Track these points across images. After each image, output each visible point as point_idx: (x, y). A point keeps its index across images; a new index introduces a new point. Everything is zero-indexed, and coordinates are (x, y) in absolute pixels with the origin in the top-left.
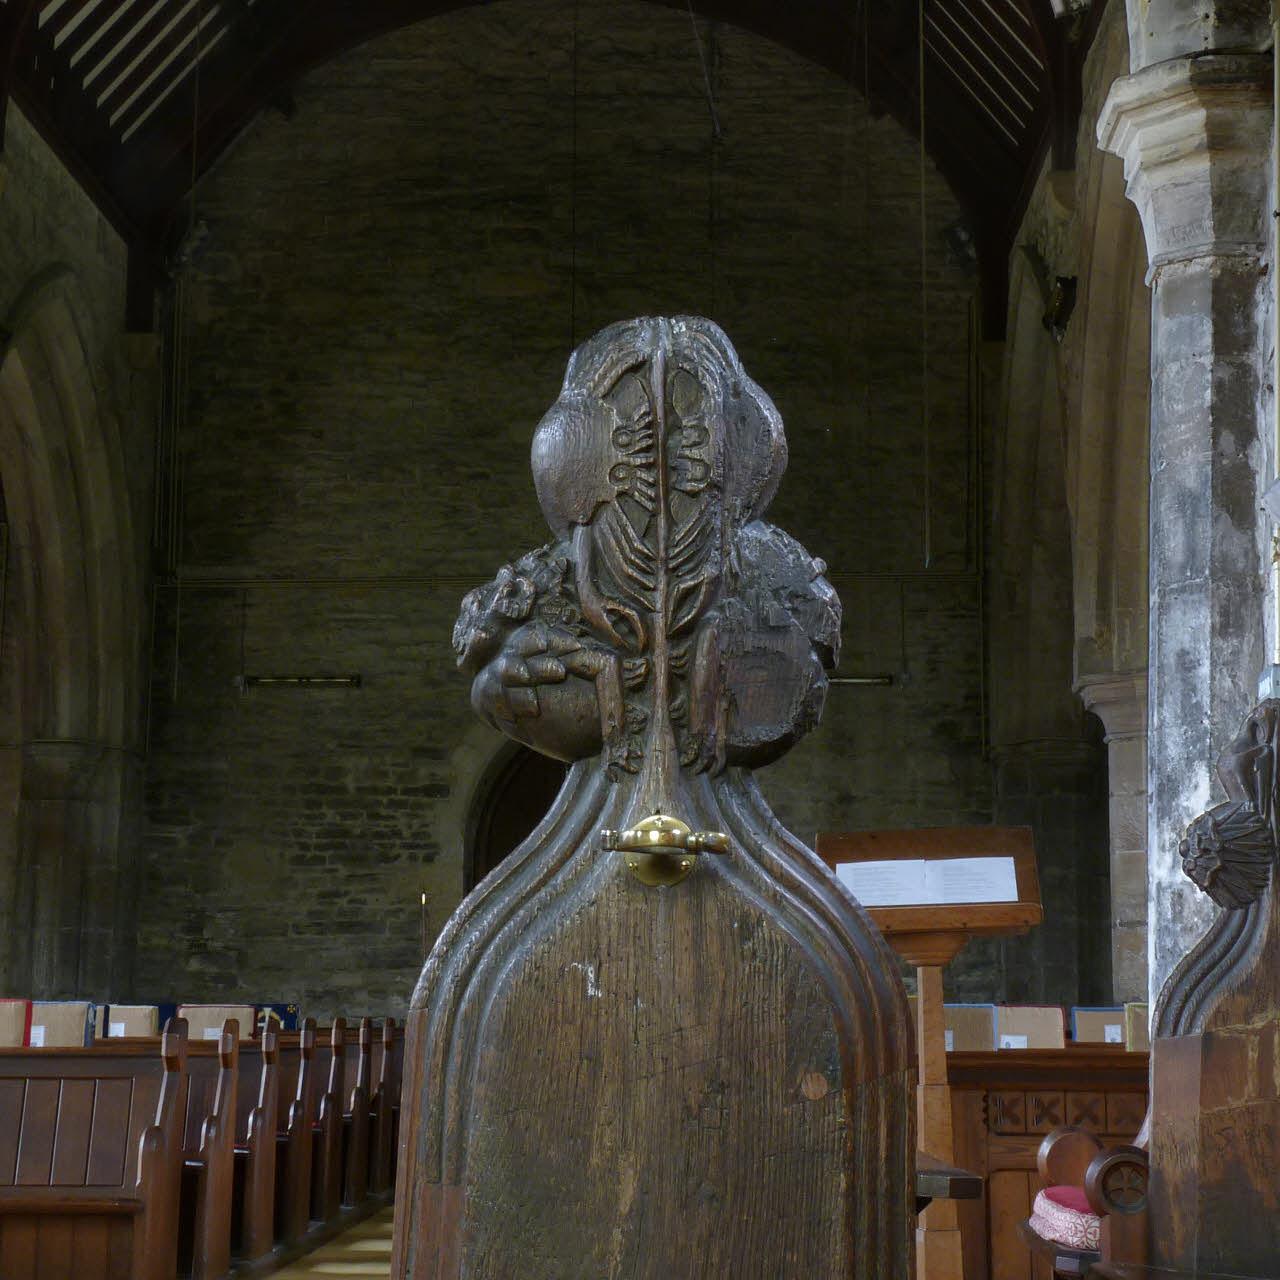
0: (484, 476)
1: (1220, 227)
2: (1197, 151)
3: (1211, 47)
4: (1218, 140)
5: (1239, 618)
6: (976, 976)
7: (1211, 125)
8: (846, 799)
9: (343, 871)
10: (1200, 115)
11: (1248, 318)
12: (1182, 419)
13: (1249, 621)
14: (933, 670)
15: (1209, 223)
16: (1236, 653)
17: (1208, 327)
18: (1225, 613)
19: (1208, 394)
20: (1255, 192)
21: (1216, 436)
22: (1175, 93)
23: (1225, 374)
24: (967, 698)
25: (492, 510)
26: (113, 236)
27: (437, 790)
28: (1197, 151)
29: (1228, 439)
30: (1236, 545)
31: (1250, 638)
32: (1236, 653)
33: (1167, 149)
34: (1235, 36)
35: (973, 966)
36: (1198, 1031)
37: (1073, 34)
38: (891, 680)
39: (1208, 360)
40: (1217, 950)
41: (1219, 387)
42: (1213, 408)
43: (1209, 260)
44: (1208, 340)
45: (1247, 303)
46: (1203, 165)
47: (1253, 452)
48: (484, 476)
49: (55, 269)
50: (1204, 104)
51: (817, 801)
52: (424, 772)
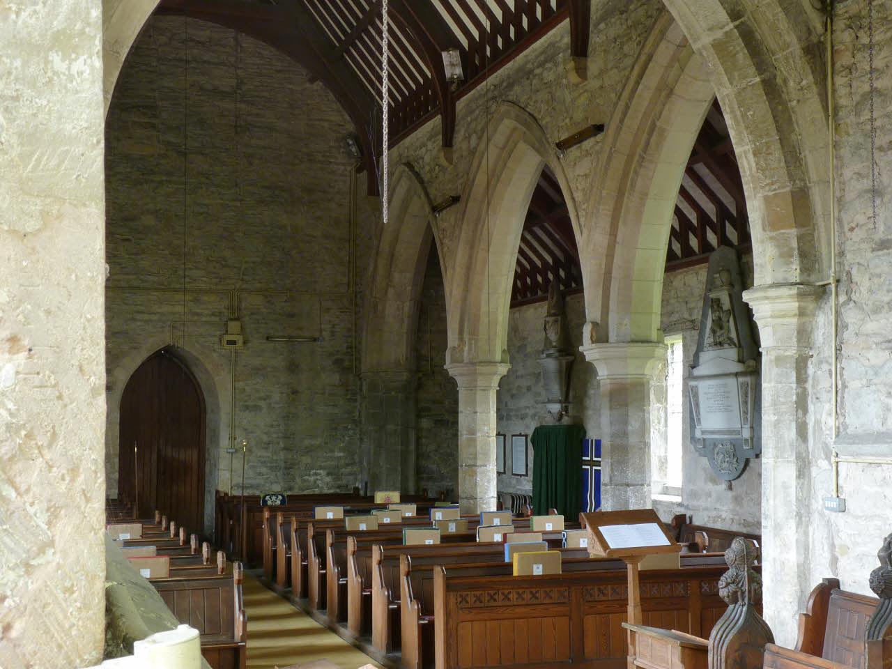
0: (128, 240)
1: (799, 341)
2: (795, 315)
3: (798, 281)
4: (802, 313)
5: (804, 473)
6: (349, 469)
7: (799, 308)
8: (295, 392)
10: (797, 304)
11: (806, 372)
12: (783, 404)
13: (807, 474)
14: (333, 336)
15: (795, 340)
16: (803, 484)
17: (794, 374)
18: (799, 471)
19: (794, 398)
20: (809, 330)
21: (797, 411)
22: (791, 296)
23: (800, 390)
24: (347, 348)
25: (133, 257)
28: (795, 315)
29: (800, 412)
30: (803, 446)
31: (807, 479)
32: (803, 484)
33: (783, 313)
34: (805, 278)
35: (348, 465)
36: (880, 639)
37: (453, 88)
38: (315, 340)
39: (794, 386)
40: (882, 611)
41: (797, 395)
42: (796, 403)
43: (794, 352)
44: (794, 379)
45: (806, 366)
46: (795, 320)
47: (808, 417)
48: (128, 240)
50: (798, 301)
51: (282, 393)
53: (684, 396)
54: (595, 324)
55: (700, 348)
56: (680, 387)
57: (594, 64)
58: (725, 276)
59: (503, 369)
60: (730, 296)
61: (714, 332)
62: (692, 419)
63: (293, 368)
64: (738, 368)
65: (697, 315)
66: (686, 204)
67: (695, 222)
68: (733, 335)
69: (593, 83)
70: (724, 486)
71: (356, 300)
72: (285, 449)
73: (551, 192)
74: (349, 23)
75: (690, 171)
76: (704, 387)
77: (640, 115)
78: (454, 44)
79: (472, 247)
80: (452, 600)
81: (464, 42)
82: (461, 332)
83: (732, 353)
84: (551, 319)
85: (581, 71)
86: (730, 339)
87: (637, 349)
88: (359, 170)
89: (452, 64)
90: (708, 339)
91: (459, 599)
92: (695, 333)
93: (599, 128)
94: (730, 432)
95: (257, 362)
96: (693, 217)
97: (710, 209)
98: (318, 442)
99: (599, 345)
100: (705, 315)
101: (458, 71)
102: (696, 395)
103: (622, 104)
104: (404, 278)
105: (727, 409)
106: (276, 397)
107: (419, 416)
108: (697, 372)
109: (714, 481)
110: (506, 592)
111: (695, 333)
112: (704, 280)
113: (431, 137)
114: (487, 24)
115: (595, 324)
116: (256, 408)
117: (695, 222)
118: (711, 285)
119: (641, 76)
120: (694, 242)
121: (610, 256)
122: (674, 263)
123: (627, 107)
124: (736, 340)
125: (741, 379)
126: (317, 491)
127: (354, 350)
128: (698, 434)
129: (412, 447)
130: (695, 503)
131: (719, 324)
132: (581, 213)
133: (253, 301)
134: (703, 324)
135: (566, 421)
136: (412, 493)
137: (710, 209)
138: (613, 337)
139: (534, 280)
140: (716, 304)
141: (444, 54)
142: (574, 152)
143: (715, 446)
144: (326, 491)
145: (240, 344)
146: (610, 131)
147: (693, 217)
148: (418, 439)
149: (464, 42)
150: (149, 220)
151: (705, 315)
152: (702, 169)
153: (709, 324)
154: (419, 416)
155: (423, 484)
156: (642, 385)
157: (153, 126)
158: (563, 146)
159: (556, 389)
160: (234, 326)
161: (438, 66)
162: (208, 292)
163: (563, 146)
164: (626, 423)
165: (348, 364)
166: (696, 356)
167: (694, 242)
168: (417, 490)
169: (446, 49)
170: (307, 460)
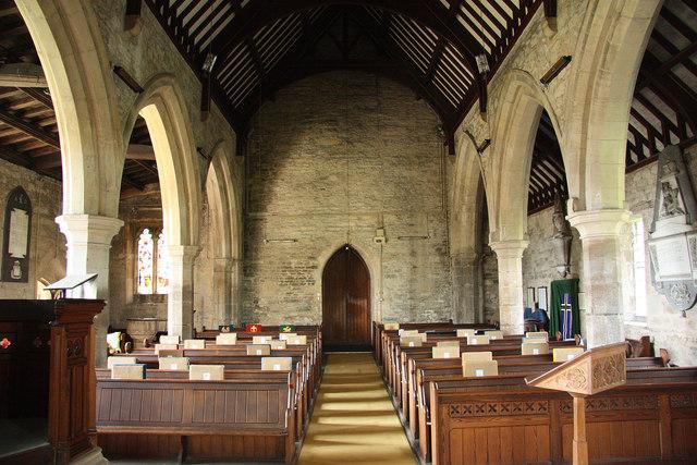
9: (292, 287)
26: (233, 132)
27: (314, 267)
49: (221, 141)
52: (311, 263)
53: (646, 254)
54: (576, 199)
55: (656, 218)
56: (643, 250)
57: (561, 20)
58: (672, 165)
59: (525, 245)
60: (677, 179)
61: (666, 205)
62: (652, 269)
63: (413, 254)
64: (688, 228)
65: (652, 197)
66: (639, 123)
67: (646, 137)
68: (681, 206)
69: (562, 31)
70: (680, 314)
71: (445, 215)
72: (411, 298)
73: (546, 131)
74: (461, 93)
75: (638, 95)
76: (658, 245)
77: (597, 40)
78: (481, 51)
79: (500, 169)
80: (445, 410)
81: (488, 49)
82: (497, 223)
83: (681, 218)
84: (557, 215)
85: (553, 26)
86: (680, 209)
87: (608, 214)
88: (445, 145)
89: (482, 64)
90: (662, 211)
91: (451, 410)
92: (652, 211)
93: (568, 59)
94: (682, 276)
95: (393, 251)
96: (644, 133)
97: (656, 123)
98: (427, 295)
99: (580, 213)
100: (658, 196)
101: (487, 67)
102: (655, 252)
103: (582, 35)
104: (469, 199)
105: (679, 259)
106: (405, 270)
107: (484, 279)
108: (654, 236)
109: (671, 311)
110: (480, 405)
111: (652, 211)
112: (656, 172)
113: (476, 110)
114: (498, 32)
115: (576, 199)
116: (394, 276)
117: (646, 137)
118: (661, 174)
119: (594, 10)
120: (647, 152)
121: (583, 149)
122: (631, 167)
123: (587, 36)
124: (683, 209)
125: (690, 237)
126: (429, 322)
127: (447, 243)
128: (657, 279)
129: (481, 296)
130: (656, 326)
131: (669, 199)
132: (561, 122)
133: (390, 219)
134: (657, 202)
135: (569, 277)
136: (481, 322)
137: (656, 123)
138: (589, 206)
139: (547, 195)
140: (667, 186)
141: (477, 58)
142: (554, 82)
143: (671, 287)
144: (434, 321)
145: (383, 242)
146: (575, 59)
147: (644, 133)
148: (484, 292)
149: (488, 49)
150: (334, 178)
151: (658, 196)
152: (650, 95)
153: (662, 201)
154: (484, 279)
155: (488, 317)
156: (614, 241)
157: (335, 130)
158: (546, 80)
159: (562, 258)
160: (380, 232)
161: (474, 67)
162: (366, 214)
163: (546, 80)
164: (602, 269)
165: (443, 250)
166: (653, 225)
167: (647, 152)
168: (484, 319)
169: (478, 54)
170: (422, 304)
